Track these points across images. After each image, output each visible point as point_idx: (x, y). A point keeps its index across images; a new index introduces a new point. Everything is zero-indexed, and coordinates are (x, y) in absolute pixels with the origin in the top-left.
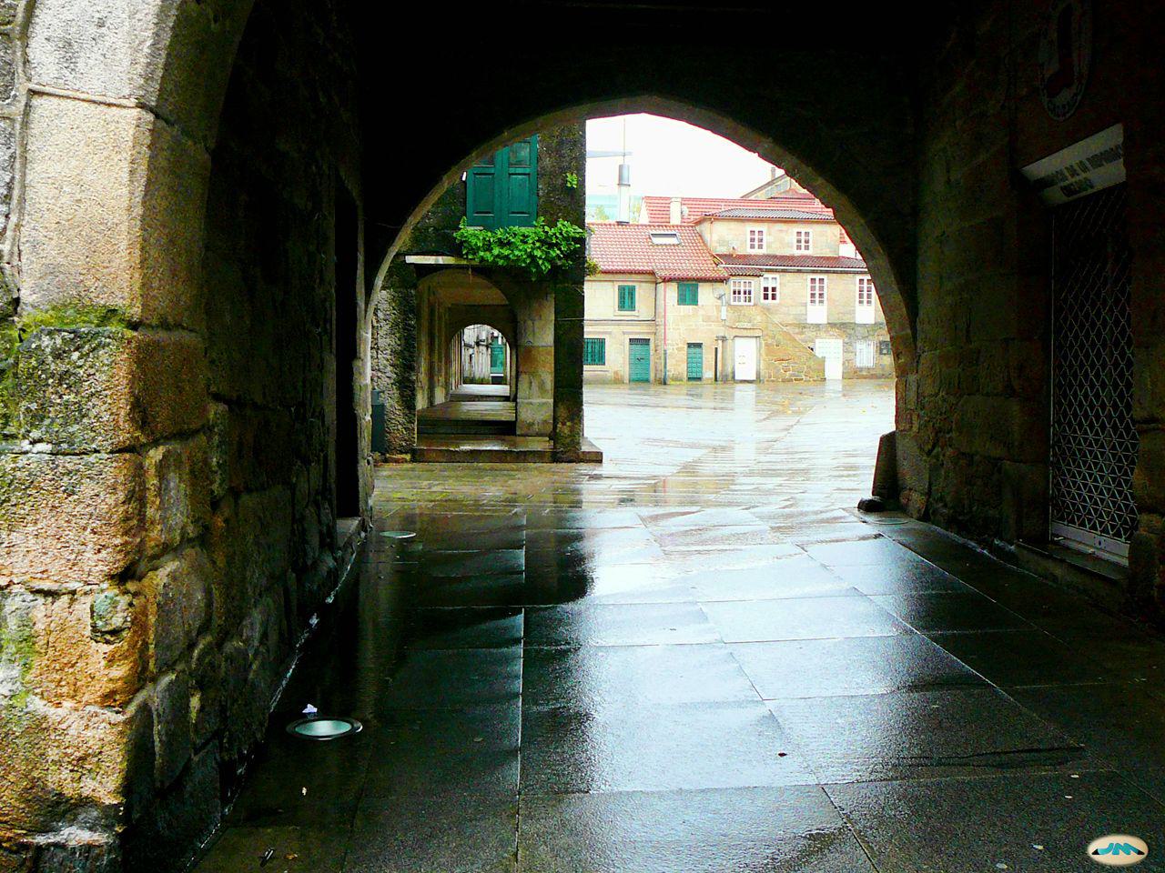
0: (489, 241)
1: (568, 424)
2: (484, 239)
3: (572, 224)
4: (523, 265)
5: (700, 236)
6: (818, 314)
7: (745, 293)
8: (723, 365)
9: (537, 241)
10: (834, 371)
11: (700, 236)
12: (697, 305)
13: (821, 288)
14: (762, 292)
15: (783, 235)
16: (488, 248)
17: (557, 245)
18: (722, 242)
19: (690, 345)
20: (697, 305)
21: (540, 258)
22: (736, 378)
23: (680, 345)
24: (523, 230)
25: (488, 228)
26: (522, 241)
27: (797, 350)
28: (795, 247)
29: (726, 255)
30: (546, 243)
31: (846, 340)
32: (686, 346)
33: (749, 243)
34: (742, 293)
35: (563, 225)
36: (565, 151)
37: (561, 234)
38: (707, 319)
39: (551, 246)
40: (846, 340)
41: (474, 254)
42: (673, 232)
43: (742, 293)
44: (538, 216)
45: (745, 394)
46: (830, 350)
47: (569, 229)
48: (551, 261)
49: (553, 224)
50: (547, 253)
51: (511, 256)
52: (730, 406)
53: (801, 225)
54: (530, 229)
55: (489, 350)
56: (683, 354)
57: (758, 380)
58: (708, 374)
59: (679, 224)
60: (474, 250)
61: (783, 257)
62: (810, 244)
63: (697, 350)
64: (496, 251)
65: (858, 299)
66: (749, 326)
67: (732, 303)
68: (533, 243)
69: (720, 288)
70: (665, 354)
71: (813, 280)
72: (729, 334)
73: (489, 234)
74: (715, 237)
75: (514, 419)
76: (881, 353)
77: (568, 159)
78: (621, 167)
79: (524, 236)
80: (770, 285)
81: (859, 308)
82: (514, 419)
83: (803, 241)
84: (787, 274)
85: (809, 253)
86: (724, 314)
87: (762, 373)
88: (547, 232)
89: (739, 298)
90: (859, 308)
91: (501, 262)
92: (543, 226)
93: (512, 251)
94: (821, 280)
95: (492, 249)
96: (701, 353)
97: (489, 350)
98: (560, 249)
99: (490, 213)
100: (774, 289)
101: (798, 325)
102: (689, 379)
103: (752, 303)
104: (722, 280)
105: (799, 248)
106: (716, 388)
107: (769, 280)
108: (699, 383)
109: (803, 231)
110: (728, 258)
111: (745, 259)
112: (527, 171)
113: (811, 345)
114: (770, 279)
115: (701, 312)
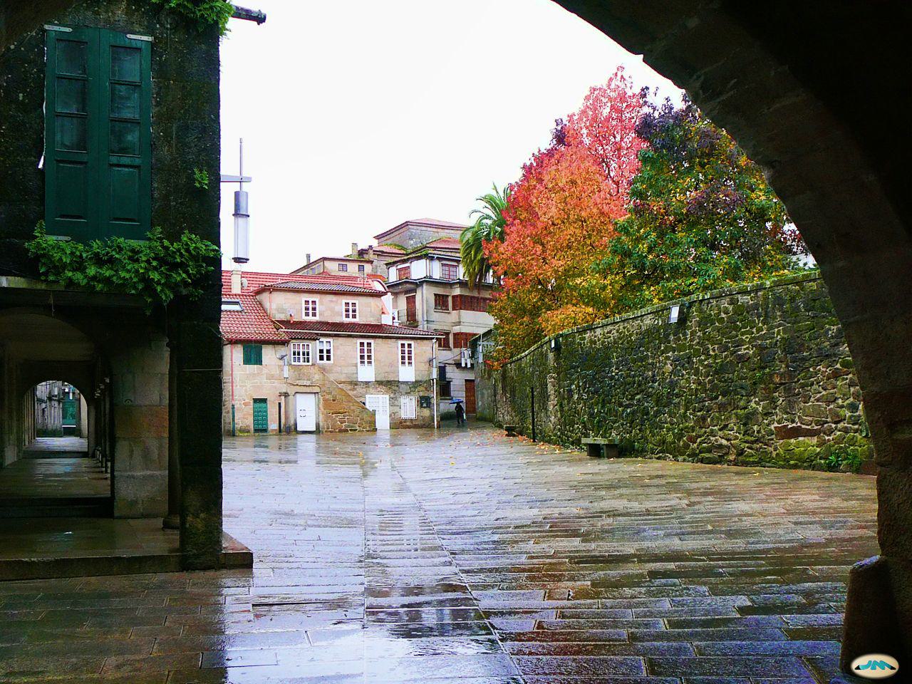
0: (81, 256)
1: (202, 515)
2: (72, 253)
3: (202, 239)
4: (133, 292)
5: (260, 304)
6: (367, 373)
7: (304, 354)
8: (287, 418)
9: (154, 259)
10: (383, 422)
11: (260, 304)
12: (262, 365)
13: (369, 351)
14: (318, 354)
15: (333, 305)
16: (79, 265)
17: (183, 266)
18: (281, 310)
19: (256, 401)
20: (262, 365)
21: (159, 283)
22: (299, 429)
23: (247, 401)
24: (134, 243)
25: (78, 238)
26: (130, 258)
27: (351, 404)
28: (344, 316)
29: (284, 321)
30: (167, 263)
31: (392, 395)
32: (252, 402)
33: (304, 311)
34: (301, 354)
35: (191, 239)
36: (191, 138)
37: (188, 250)
38: (271, 377)
39: (174, 267)
40: (392, 395)
41: (58, 274)
42: (236, 300)
43: (301, 354)
44: (152, 225)
45: (307, 445)
46: (378, 403)
47: (199, 245)
48: (173, 287)
49: (175, 237)
50: (168, 277)
51: (114, 279)
52: (292, 457)
53: (348, 297)
54: (142, 243)
55: (61, 404)
56: (250, 409)
57: (318, 431)
58: (273, 426)
59: (240, 293)
60: (59, 268)
61: (334, 323)
62: (357, 313)
63: (263, 405)
64: (92, 271)
65: (400, 361)
66: (308, 383)
67: (293, 363)
68: (148, 262)
69: (282, 350)
70: (233, 408)
71: (362, 344)
72: (291, 390)
73: (81, 247)
74: (274, 306)
75: (108, 494)
76: (422, 407)
77: (195, 150)
78: (237, 195)
79: (133, 251)
80: (325, 347)
81: (401, 368)
82: (108, 494)
83: (351, 311)
84: (340, 339)
85: (356, 320)
86: (286, 372)
87: (321, 424)
88: (166, 248)
89: (299, 358)
90: (401, 368)
91: (99, 287)
92: (161, 239)
93: (116, 271)
94: (369, 344)
95: (85, 268)
96: (266, 408)
97: (61, 404)
98: (186, 272)
99: (81, 218)
100: (328, 351)
101: (351, 383)
102: (256, 430)
103: (310, 363)
104: (284, 343)
105: (347, 316)
106: (281, 440)
107: (324, 344)
108: (265, 434)
109: (350, 302)
110: (286, 323)
111: (301, 324)
112: (137, 162)
113: (362, 399)
114: (325, 342)
115: (265, 371)
